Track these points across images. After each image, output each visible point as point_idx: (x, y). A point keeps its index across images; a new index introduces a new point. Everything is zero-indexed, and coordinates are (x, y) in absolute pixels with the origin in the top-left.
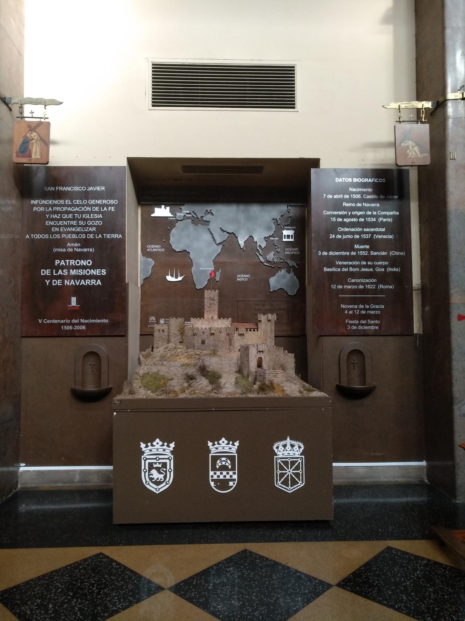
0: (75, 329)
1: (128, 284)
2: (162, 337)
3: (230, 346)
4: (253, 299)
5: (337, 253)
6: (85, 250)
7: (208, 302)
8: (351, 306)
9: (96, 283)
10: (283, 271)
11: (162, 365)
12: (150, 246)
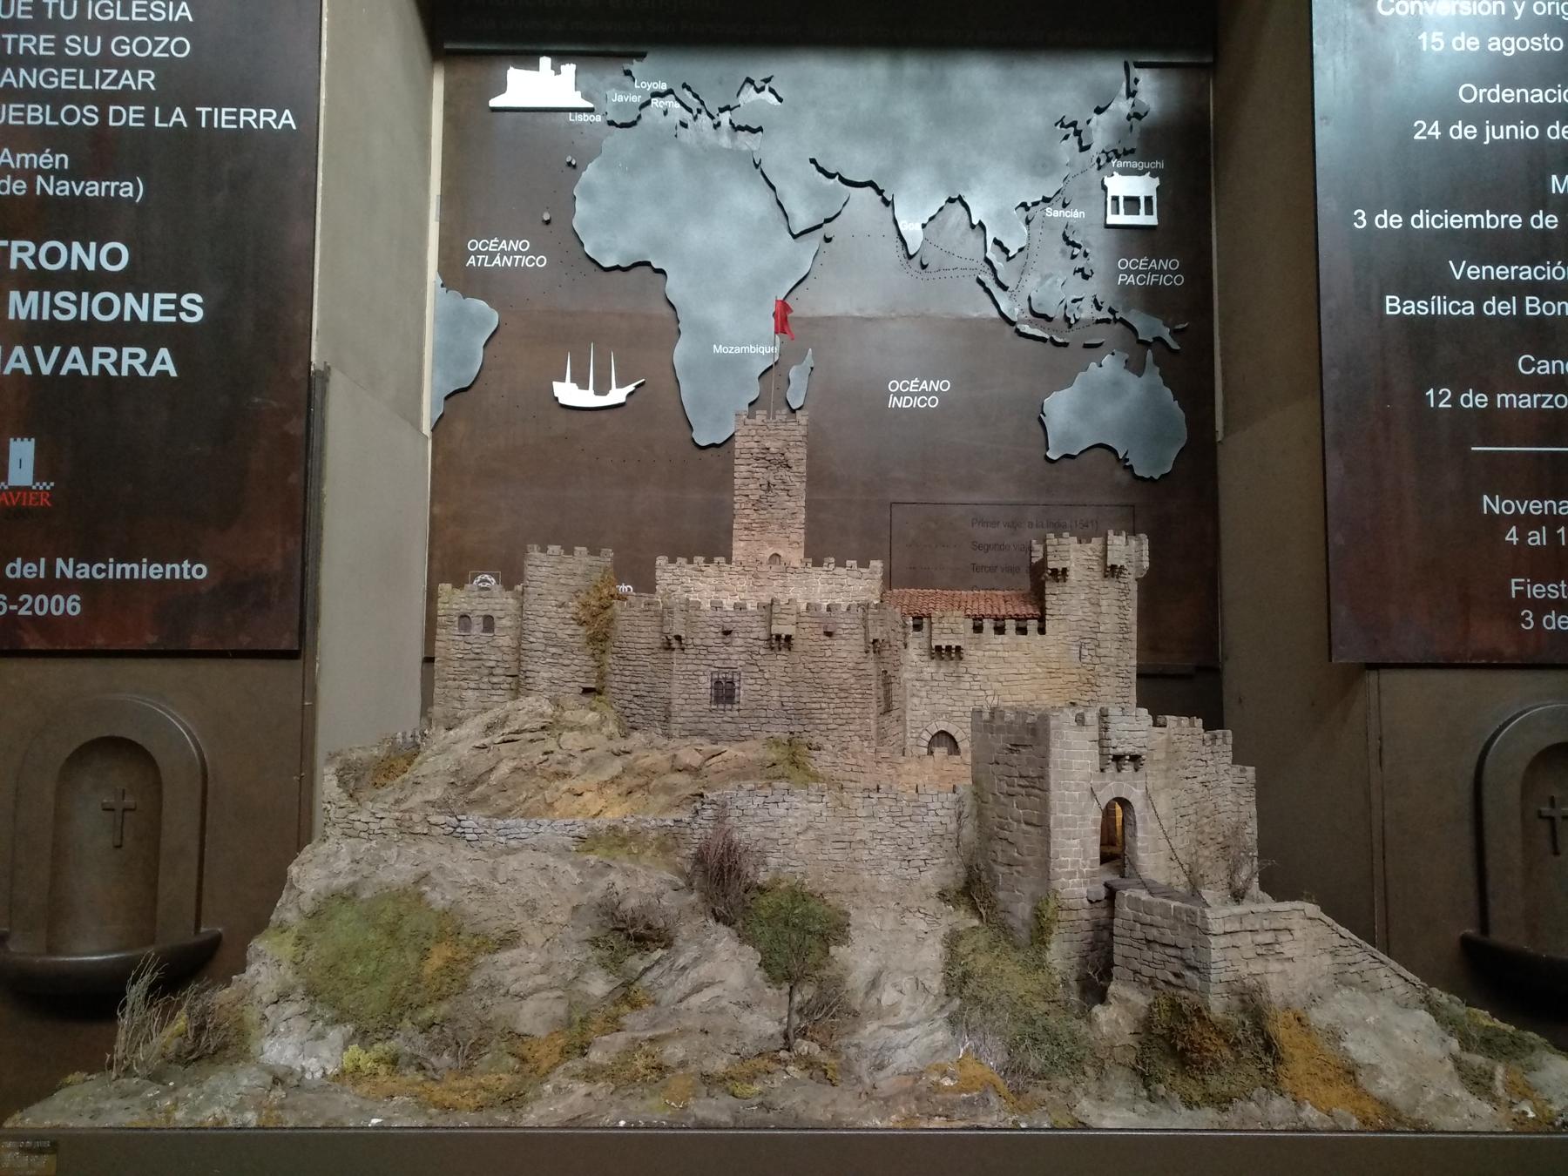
0: (22, 612)
1: (324, 376)
2: (478, 657)
3: (886, 720)
4: (961, 497)
5: (1455, 221)
6: (95, 189)
7: (751, 476)
8: (1535, 507)
9: (147, 365)
10: (1108, 366)
11: (456, 834)
12: (479, 245)
